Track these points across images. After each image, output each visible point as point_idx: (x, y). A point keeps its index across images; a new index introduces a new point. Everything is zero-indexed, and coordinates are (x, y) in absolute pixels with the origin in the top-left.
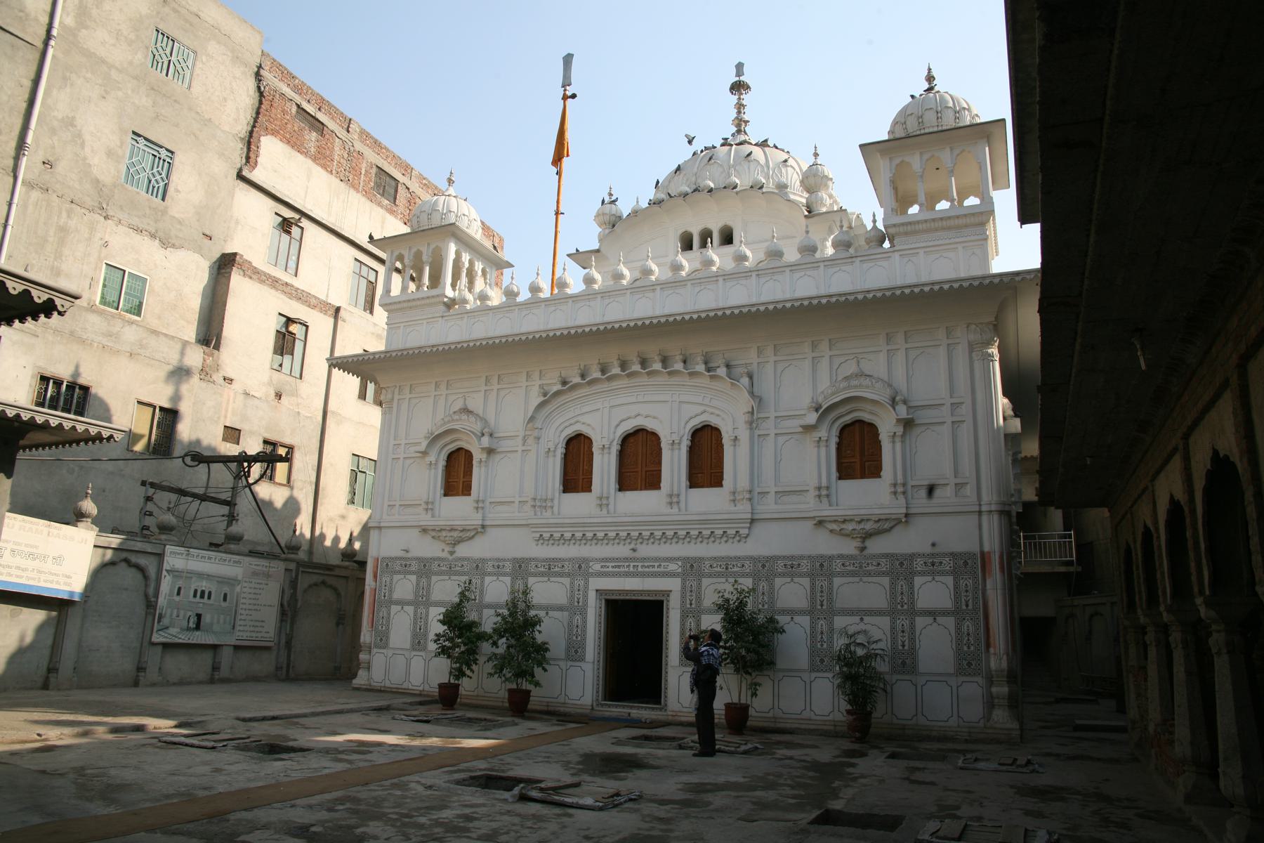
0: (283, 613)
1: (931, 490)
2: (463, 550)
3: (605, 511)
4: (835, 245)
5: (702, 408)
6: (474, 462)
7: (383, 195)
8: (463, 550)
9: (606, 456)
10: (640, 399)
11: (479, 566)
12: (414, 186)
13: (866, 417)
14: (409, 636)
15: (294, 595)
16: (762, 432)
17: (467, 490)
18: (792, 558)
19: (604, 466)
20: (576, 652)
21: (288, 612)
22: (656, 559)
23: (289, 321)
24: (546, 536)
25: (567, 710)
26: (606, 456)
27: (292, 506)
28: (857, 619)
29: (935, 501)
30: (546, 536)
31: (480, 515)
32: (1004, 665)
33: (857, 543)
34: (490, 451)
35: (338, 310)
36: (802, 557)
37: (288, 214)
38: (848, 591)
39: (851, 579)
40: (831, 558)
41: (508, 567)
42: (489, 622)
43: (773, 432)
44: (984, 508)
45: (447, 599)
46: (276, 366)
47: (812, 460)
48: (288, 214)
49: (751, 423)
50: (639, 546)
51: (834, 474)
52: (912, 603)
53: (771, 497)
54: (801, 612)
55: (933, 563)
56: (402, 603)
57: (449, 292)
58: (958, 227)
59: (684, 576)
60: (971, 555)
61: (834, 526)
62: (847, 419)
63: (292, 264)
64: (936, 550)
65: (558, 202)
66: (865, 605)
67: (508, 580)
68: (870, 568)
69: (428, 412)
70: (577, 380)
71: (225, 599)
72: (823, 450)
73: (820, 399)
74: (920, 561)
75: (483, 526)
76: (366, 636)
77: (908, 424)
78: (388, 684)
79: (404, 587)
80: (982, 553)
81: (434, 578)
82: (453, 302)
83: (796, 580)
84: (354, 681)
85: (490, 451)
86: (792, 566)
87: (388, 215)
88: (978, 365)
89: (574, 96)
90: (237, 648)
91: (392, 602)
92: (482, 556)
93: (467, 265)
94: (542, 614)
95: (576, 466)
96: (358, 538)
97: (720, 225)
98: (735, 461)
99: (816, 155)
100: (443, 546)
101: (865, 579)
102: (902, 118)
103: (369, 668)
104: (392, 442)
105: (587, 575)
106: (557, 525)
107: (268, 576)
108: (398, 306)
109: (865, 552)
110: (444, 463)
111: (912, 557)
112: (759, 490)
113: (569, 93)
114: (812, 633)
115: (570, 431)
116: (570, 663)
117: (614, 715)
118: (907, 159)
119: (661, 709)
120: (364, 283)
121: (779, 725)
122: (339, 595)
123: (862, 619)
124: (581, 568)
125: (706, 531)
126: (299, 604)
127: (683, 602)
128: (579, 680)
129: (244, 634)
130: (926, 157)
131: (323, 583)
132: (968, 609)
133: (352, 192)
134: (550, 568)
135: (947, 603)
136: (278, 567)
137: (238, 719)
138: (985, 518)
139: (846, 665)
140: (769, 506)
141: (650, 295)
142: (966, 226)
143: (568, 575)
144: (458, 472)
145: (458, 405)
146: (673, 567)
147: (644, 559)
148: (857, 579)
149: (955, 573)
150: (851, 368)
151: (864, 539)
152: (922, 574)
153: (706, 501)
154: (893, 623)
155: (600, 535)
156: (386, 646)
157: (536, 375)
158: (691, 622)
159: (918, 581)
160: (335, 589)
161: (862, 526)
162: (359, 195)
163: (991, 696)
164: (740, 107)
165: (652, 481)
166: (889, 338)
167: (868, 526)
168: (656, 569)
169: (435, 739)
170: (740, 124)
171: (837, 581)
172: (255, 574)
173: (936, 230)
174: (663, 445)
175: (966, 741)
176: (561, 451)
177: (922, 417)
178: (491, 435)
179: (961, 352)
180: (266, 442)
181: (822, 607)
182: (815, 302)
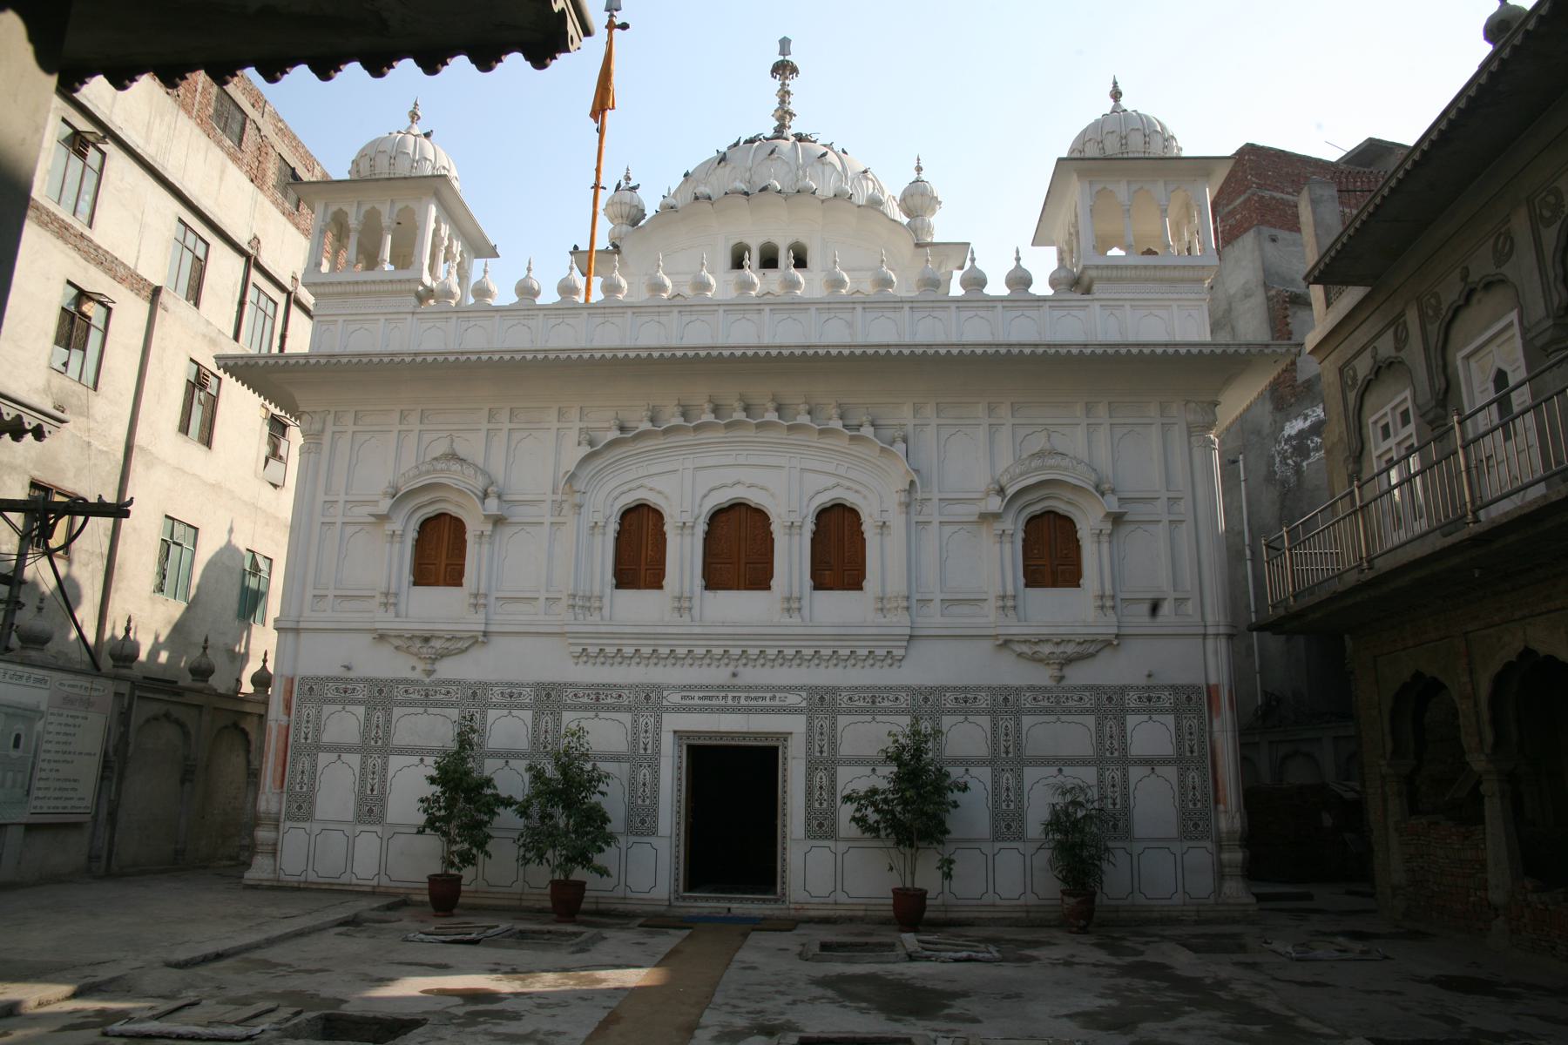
0: (106, 765)
1: (1155, 608)
2: (448, 669)
3: (687, 617)
4: (964, 283)
5: (833, 481)
6: (469, 537)
7: (224, 131)
8: (448, 669)
9: (688, 539)
10: (741, 460)
11: (477, 694)
12: (268, 129)
13: (1061, 507)
14: (351, 805)
15: (124, 736)
16: (921, 519)
17: (454, 577)
18: (966, 689)
19: (684, 553)
20: (643, 822)
21: (114, 765)
22: (768, 688)
23: (82, 295)
24: (593, 650)
25: (630, 907)
26: (688, 539)
27: (67, 594)
28: (1054, 770)
29: (1160, 619)
30: (593, 650)
31: (481, 616)
32: (1237, 824)
33: (1052, 671)
34: (498, 521)
35: (157, 291)
36: (979, 689)
37: (83, 125)
38: (1040, 734)
39: (1046, 718)
40: (1018, 690)
41: (528, 696)
42: (512, 781)
43: (936, 519)
44: (1211, 630)
45: (436, 744)
46: (58, 365)
47: (995, 561)
48: (83, 125)
49: (908, 505)
50: (740, 669)
51: (1021, 580)
52: (1124, 748)
53: (935, 607)
54: (980, 762)
55: (1149, 698)
56: (338, 749)
57: (427, 279)
58: (1172, 281)
59: (810, 712)
60: (1195, 689)
61: (1025, 648)
62: (1037, 508)
63: (85, 207)
64: (1152, 682)
65: (598, 170)
66: (1066, 751)
67: (528, 715)
68: (1071, 703)
69: (389, 456)
70: (646, 426)
71: (16, 745)
72: (1007, 547)
73: (1004, 480)
74: (1133, 695)
75: (485, 634)
76: (269, 800)
77: (1117, 519)
78: (312, 877)
79: (344, 724)
80: (1208, 687)
81: (397, 712)
82: (430, 292)
83: (971, 718)
84: (247, 875)
85: (498, 521)
86: (965, 700)
87: (229, 163)
88: (1198, 454)
89: (624, 26)
90: (30, 828)
91: (319, 747)
92: (1122, 682)
93: (446, 243)
94: (604, 767)
95: (638, 550)
96: (165, 646)
97: (790, 241)
98: (884, 556)
99: (919, 169)
100: (413, 661)
101: (1063, 718)
102: (1084, 138)
103: (274, 853)
104: (321, 497)
105: (660, 710)
106: (613, 635)
107: (88, 704)
108: (339, 289)
109: (1064, 683)
110: (415, 535)
111: (1123, 689)
112: (919, 596)
113: (618, 21)
114: (994, 789)
115: (629, 500)
116: (633, 839)
117: (705, 912)
118: (1110, 187)
119: (776, 901)
120: (188, 257)
121: (951, 915)
122: (186, 734)
123: (1060, 771)
124: (649, 699)
125: (842, 647)
126: (131, 748)
127: (809, 750)
128: (650, 864)
129: (45, 803)
130: (1098, 187)
131: (167, 716)
132: (1192, 756)
133: (182, 115)
134: (599, 698)
135: (1168, 749)
136: (103, 691)
137: (169, 965)
138: (1210, 643)
139: (1058, 831)
140: (933, 619)
141: (755, 317)
142: (1182, 280)
143: (629, 709)
144: (439, 550)
145: (441, 448)
146: (793, 699)
147: (749, 688)
148: (1053, 718)
149: (1176, 710)
150: (1039, 442)
151: (1062, 666)
152: (1137, 711)
153: (836, 607)
154: (1100, 775)
155: (681, 651)
156: (309, 817)
157: (574, 414)
158: (821, 777)
159: (1131, 720)
160: (181, 725)
161: (1061, 649)
162: (192, 123)
163: (1221, 864)
164: (784, 94)
165: (759, 578)
166: (1089, 409)
167: (1070, 649)
168: (768, 702)
169: (550, 977)
170: (784, 115)
171: (1027, 721)
172: (68, 701)
173: (1146, 280)
174: (773, 527)
175: (1197, 923)
176: (613, 527)
177: (1135, 511)
178: (499, 497)
179: (1178, 434)
180: (34, 485)
181: (1009, 757)
182: (1015, 351)
